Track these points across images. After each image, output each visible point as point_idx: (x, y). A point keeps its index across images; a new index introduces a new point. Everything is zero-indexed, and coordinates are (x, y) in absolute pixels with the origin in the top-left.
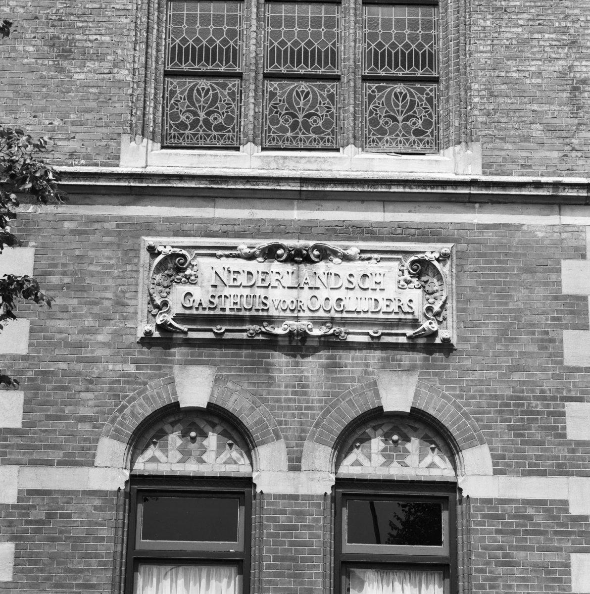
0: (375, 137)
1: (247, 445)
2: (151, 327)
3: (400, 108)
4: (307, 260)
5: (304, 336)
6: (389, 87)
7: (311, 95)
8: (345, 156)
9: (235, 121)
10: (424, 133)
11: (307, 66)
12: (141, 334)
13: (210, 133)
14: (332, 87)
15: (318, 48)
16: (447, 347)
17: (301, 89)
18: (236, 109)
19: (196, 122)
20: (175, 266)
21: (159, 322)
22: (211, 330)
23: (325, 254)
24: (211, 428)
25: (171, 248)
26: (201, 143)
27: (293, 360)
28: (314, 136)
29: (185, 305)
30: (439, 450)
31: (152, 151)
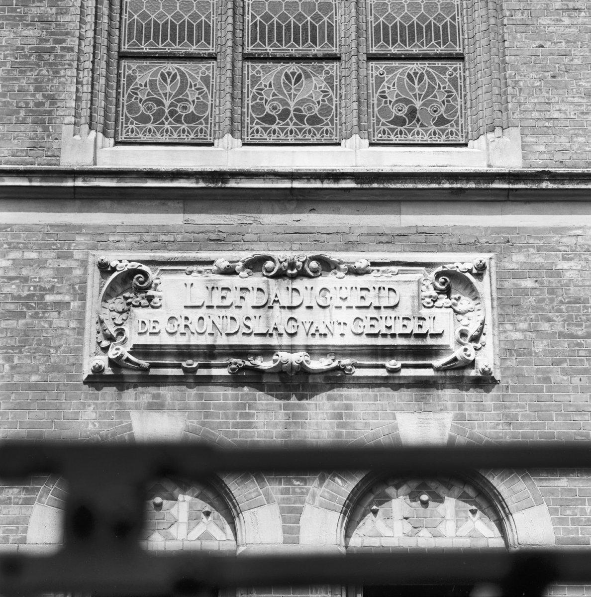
0: (258, 126)
1: (496, 512)
2: (102, 360)
3: (417, 91)
4: (302, 274)
5: (302, 371)
6: (400, 68)
7: (178, 77)
8: (347, 149)
9: (459, 113)
10: (320, 121)
11: (192, 43)
12: (87, 371)
13: (303, 126)
14: (208, 69)
15: (172, 22)
16: (485, 382)
17: (291, 70)
18: (334, 97)
19: (160, 113)
20: (130, 285)
21: (112, 357)
22: (383, 367)
23: (327, 265)
24: (446, 491)
25: (128, 263)
26: (291, 139)
27: (282, 402)
28: (308, 127)
29: (356, 332)
30: (483, 511)
31: (102, 147)
